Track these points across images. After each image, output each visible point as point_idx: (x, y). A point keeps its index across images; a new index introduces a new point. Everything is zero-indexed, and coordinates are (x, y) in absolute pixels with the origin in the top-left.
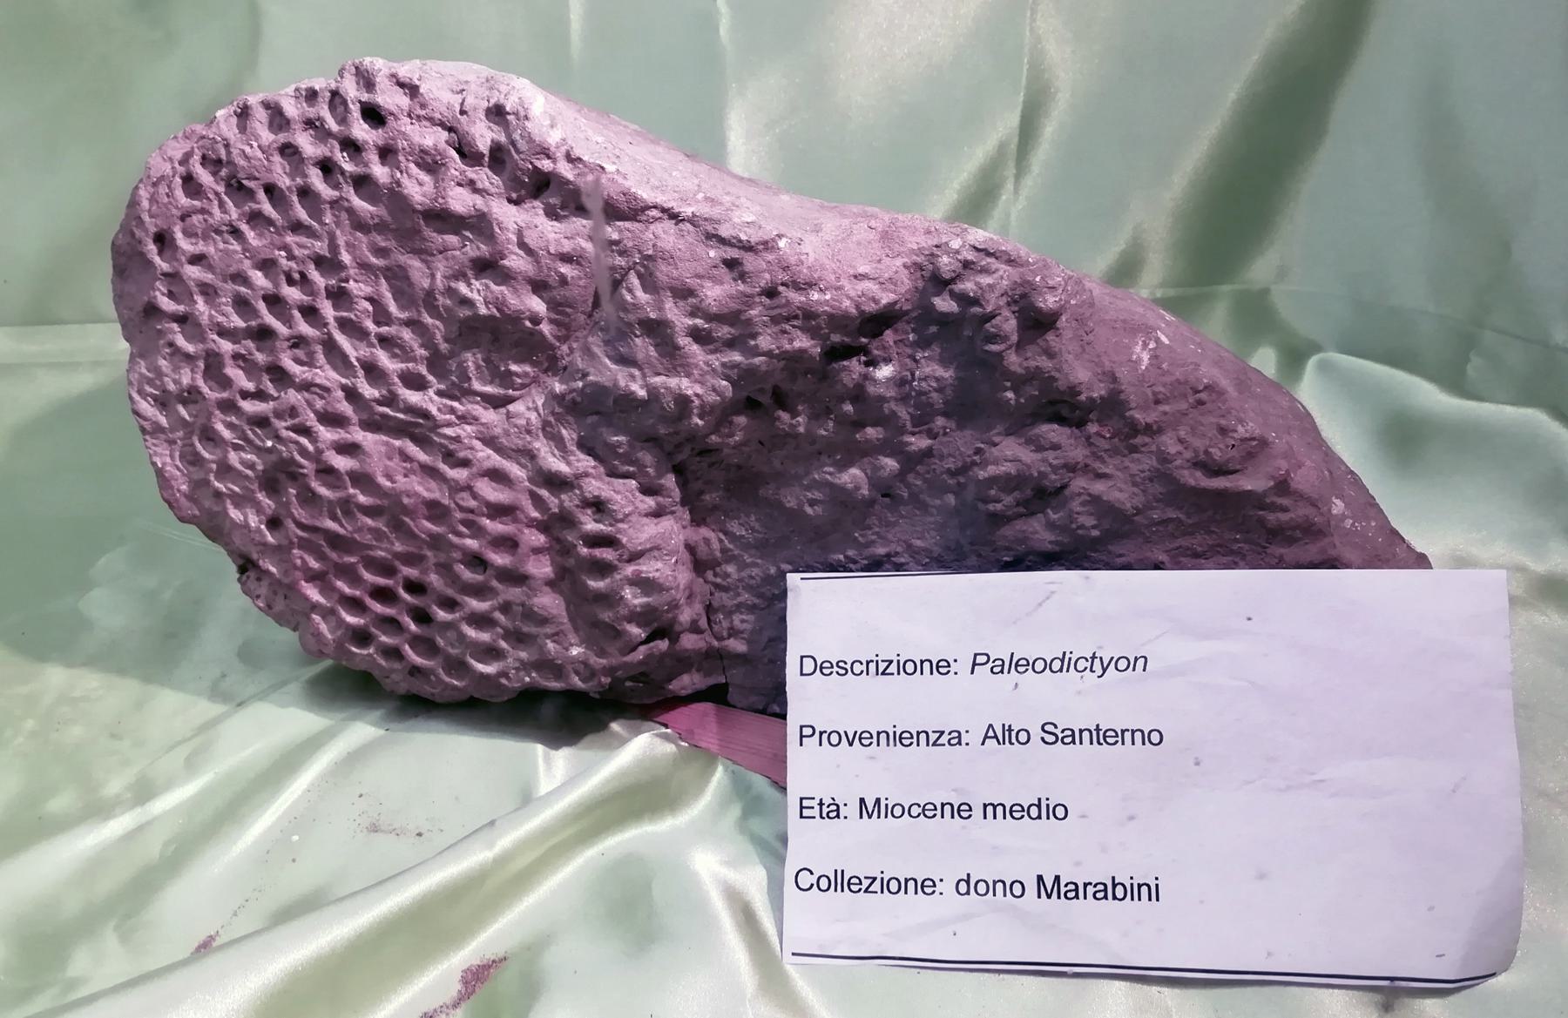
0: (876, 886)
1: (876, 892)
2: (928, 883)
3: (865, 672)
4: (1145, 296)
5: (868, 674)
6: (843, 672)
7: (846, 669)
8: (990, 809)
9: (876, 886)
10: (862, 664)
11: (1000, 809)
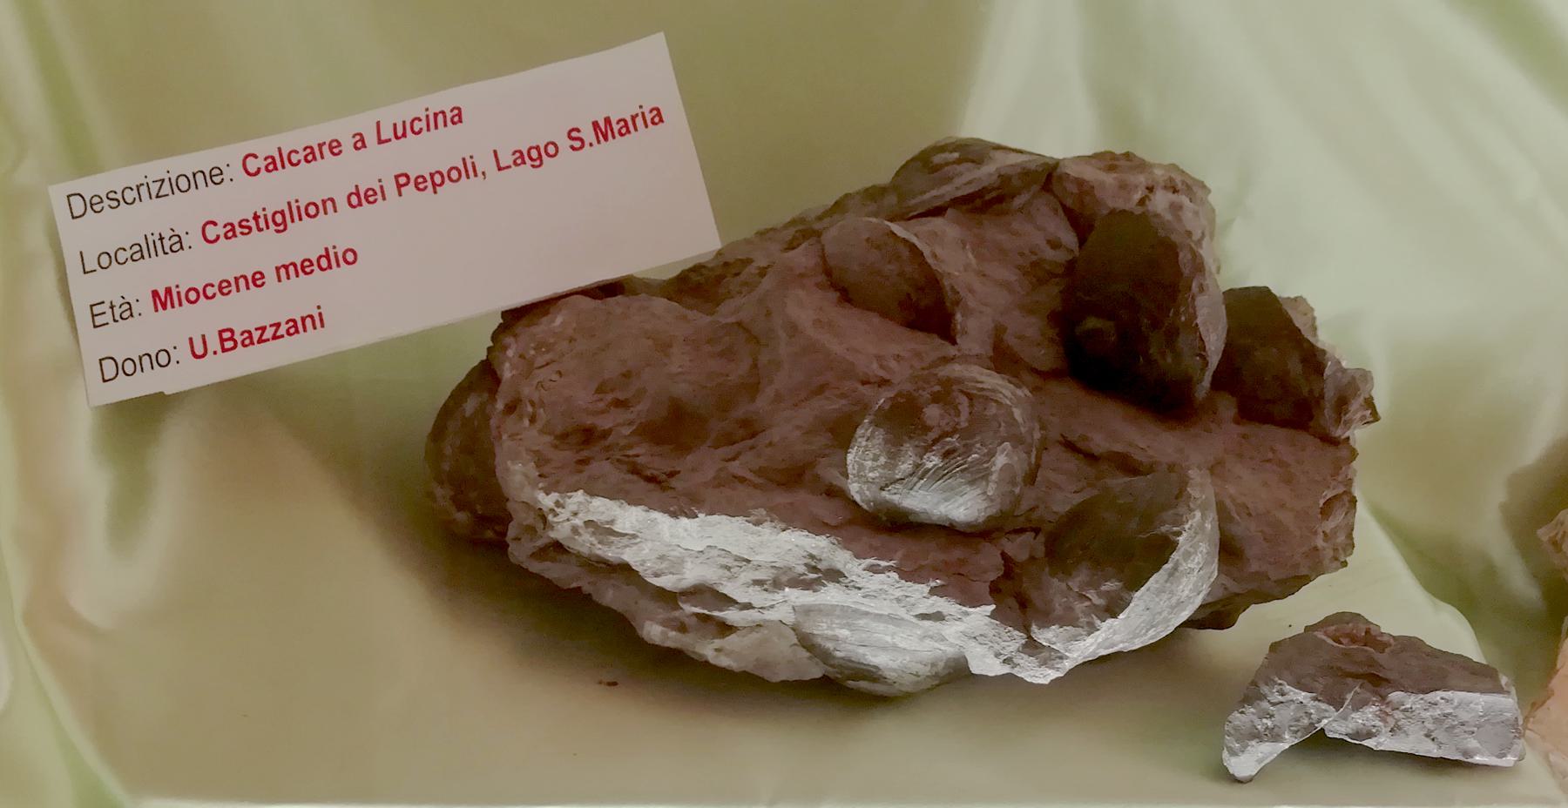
0: (166, 189)
1: (167, 195)
2: (216, 172)
3: (137, 199)
4: (489, 531)
5: (141, 200)
6: (115, 204)
7: (117, 200)
8: (283, 271)
9: (166, 189)
10: (132, 189)
11: (291, 269)
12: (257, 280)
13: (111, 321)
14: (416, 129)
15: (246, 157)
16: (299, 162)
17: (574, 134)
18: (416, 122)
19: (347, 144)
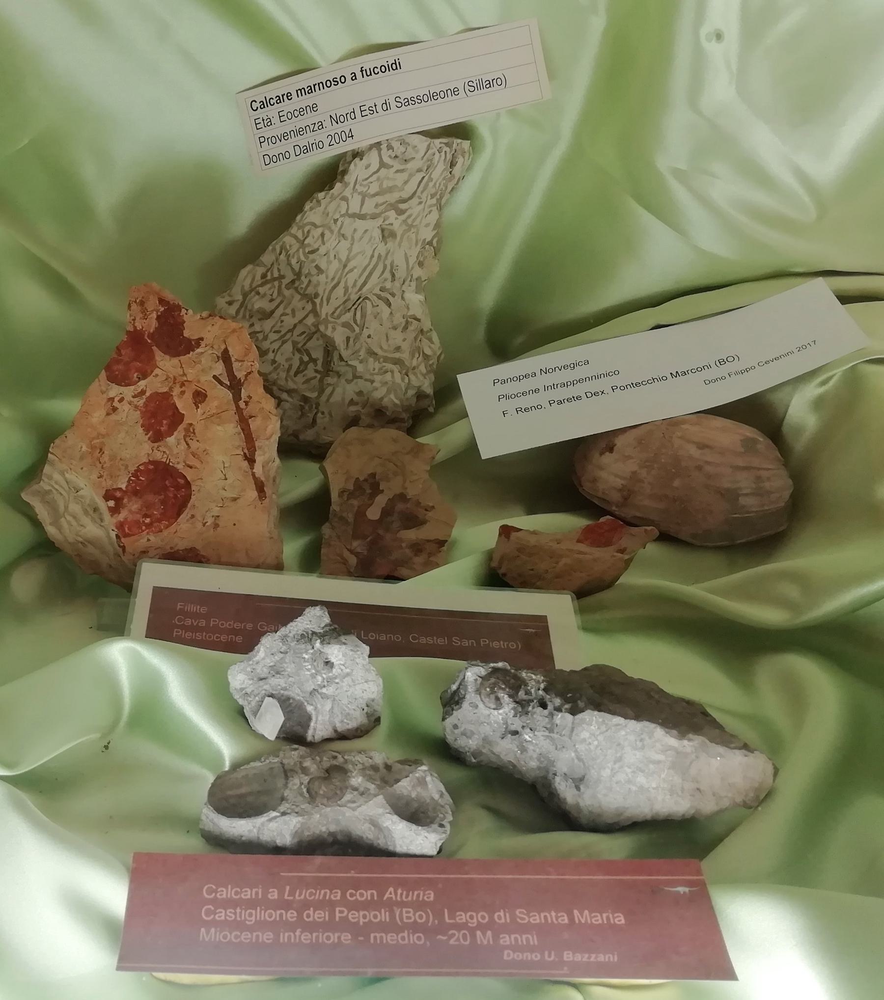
8: (299, 92)
12: (536, 391)
13: (263, 127)
14: (376, 72)
15: (252, 102)
16: (378, 73)
17: (336, 83)
18: (375, 69)
19: (349, 77)
